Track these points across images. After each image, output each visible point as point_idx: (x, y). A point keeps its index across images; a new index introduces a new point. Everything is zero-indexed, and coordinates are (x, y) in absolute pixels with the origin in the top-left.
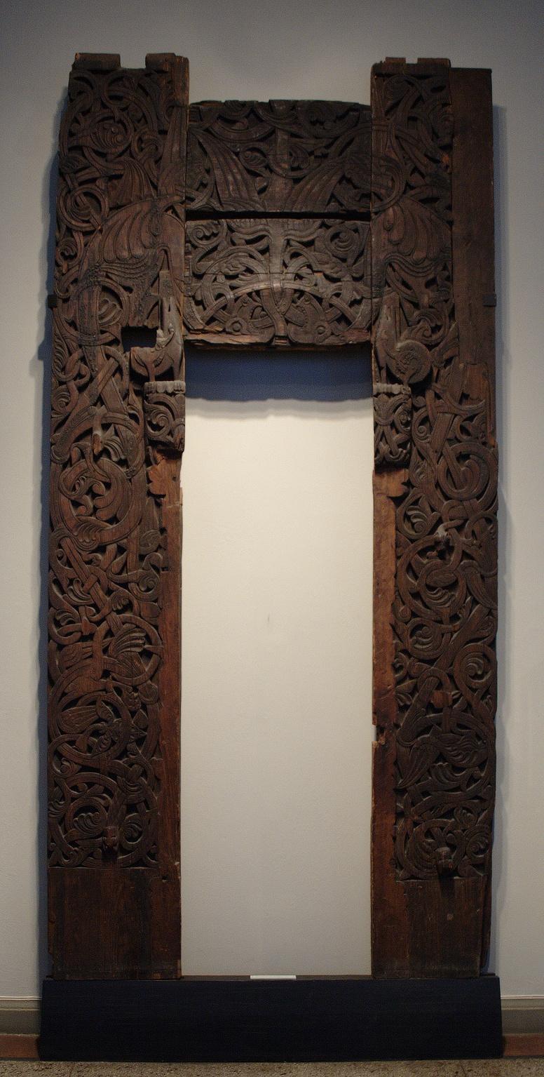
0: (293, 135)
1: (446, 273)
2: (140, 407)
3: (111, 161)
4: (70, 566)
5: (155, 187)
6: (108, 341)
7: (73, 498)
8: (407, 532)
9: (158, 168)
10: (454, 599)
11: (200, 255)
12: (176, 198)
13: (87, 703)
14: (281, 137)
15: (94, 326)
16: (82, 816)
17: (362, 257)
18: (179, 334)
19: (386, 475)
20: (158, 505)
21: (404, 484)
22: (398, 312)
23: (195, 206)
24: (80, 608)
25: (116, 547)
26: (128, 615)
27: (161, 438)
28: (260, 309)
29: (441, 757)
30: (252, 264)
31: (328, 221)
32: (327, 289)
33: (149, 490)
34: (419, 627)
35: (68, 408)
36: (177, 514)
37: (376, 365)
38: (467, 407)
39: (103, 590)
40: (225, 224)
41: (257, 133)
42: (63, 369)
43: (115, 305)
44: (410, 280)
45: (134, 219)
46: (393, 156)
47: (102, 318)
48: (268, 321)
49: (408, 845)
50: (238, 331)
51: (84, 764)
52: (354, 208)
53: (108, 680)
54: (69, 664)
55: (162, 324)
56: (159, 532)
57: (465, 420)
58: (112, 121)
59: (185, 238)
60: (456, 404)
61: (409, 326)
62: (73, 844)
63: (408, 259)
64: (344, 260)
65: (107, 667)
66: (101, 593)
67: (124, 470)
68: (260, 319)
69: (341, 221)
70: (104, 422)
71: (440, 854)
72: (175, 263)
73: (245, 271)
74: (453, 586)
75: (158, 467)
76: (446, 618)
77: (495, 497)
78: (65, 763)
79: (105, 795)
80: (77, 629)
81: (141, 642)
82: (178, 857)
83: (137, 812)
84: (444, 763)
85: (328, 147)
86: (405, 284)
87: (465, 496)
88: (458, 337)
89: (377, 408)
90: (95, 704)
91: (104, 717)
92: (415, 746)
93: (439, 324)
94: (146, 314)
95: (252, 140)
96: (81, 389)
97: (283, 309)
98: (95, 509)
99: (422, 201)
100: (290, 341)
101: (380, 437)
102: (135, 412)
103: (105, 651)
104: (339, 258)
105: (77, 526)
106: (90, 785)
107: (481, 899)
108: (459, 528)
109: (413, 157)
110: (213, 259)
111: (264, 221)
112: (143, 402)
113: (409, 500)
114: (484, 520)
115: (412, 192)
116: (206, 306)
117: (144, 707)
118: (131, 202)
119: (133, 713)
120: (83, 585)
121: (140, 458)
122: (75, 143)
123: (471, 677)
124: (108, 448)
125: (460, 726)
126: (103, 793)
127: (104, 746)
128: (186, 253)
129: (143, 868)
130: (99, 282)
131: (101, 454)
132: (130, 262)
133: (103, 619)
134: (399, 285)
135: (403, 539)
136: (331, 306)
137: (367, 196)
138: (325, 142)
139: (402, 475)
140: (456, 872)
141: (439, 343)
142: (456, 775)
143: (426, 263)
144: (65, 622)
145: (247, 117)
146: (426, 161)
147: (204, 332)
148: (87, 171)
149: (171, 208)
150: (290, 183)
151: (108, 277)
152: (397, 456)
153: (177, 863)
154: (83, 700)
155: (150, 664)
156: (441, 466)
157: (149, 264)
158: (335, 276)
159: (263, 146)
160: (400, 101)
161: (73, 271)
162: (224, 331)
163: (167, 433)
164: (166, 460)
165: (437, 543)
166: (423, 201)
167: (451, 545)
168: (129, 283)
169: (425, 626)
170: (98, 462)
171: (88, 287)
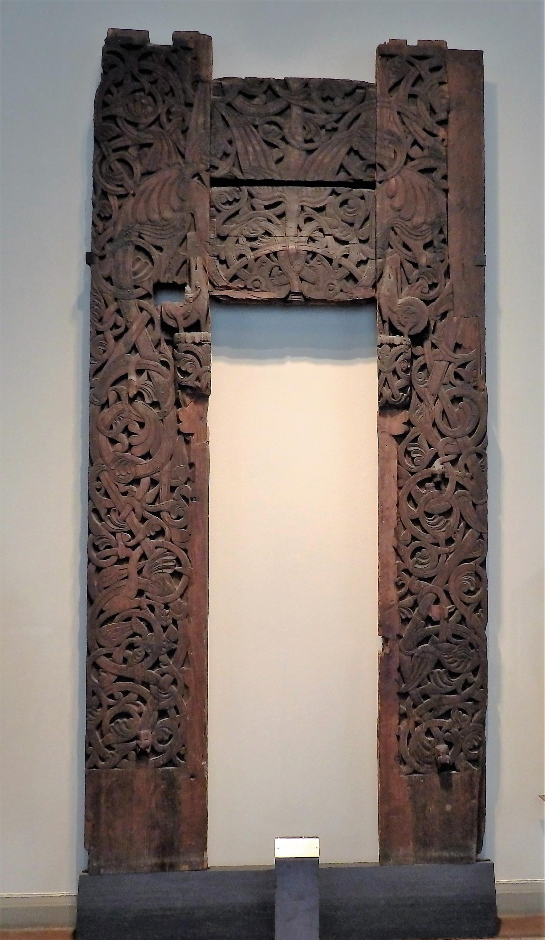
0: (306, 110)
1: (442, 237)
2: (170, 355)
3: (142, 130)
4: (108, 497)
5: (183, 156)
6: (140, 295)
7: (110, 436)
8: (407, 465)
9: (185, 137)
10: (449, 524)
11: (224, 218)
12: (202, 166)
13: (123, 619)
14: (296, 111)
15: (128, 281)
16: (118, 722)
17: (368, 222)
18: (205, 290)
19: (388, 416)
20: (187, 442)
21: (404, 423)
22: (399, 270)
23: (217, 174)
24: (117, 535)
25: (150, 479)
26: (160, 540)
27: (189, 384)
28: (278, 268)
29: (439, 664)
30: (270, 227)
31: (338, 189)
32: (337, 250)
33: (179, 429)
34: (419, 549)
35: (105, 355)
36: (205, 451)
37: (380, 318)
38: (460, 355)
39: (137, 518)
40: (246, 192)
41: (274, 107)
42: (101, 320)
43: (148, 264)
44: (411, 243)
45: (164, 185)
46: (395, 129)
47: (135, 274)
48: (284, 279)
49: (411, 744)
50: (257, 288)
51: (119, 674)
52: (361, 178)
53: (142, 598)
54: (107, 585)
55: (190, 281)
56: (188, 467)
57: (459, 367)
58: (142, 94)
59: (210, 203)
60: (451, 353)
61: (409, 284)
62: (109, 747)
63: (408, 223)
64: (352, 225)
65: (141, 587)
66: (136, 521)
67: (156, 411)
68: (277, 277)
69: (350, 189)
70: (138, 368)
71: (438, 751)
72: (200, 225)
73: (264, 234)
74: (448, 513)
75: (187, 409)
76: (442, 542)
77: (485, 434)
78: (102, 674)
79: (138, 702)
80: (114, 554)
81: (172, 564)
82: (205, 757)
83: (168, 717)
84: (441, 669)
85: (337, 121)
86: (406, 246)
87: (458, 434)
88: (452, 293)
89: (380, 357)
90: (130, 620)
91: (138, 632)
92: (416, 654)
93: (435, 281)
94: (175, 272)
95: (269, 114)
96: (117, 338)
97: (298, 268)
98: (131, 446)
99: (420, 171)
100: (304, 297)
101: (384, 383)
102: (167, 360)
103: (140, 572)
104: (347, 223)
105: (114, 461)
106: (126, 693)
107: (476, 792)
108: (454, 462)
109: (412, 130)
110: (235, 222)
111: (280, 188)
112: (173, 351)
113: (410, 437)
114: (475, 455)
115: (413, 163)
116: (229, 265)
117: (175, 622)
118: (161, 169)
119: (165, 628)
120: (119, 514)
121: (171, 400)
122: (108, 113)
123: (464, 593)
124: (142, 391)
125: (455, 636)
126: (137, 700)
127: (138, 658)
128: (212, 217)
129: (172, 768)
130: (132, 241)
131: (135, 397)
132: (161, 224)
133: (138, 544)
134: (400, 247)
135: (404, 472)
136: (340, 266)
137: (373, 166)
138: (335, 117)
139: (403, 416)
140: (453, 767)
141: (435, 299)
142: (453, 680)
143: (424, 227)
144: (104, 546)
145: (265, 93)
146: (424, 134)
147: (228, 288)
148: (120, 139)
149: (197, 175)
150: (304, 153)
151: (140, 237)
152: (398, 399)
153: (204, 763)
154: (119, 617)
155: (180, 585)
156: (438, 408)
157: (178, 226)
158: (344, 239)
159: (278, 119)
160: (403, 78)
161: (109, 230)
162: (245, 287)
163: (195, 378)
164: (195, 403)
165: (434, 476)
166: (423, 171)
167: (446, 476)
168: (159, 243)
169: (424, 548)
170: (133, 404)
171: (122, 246)
